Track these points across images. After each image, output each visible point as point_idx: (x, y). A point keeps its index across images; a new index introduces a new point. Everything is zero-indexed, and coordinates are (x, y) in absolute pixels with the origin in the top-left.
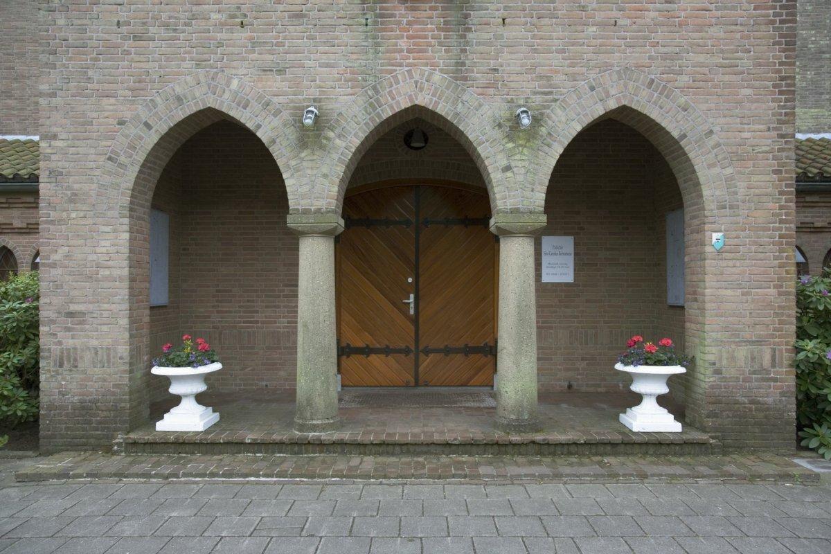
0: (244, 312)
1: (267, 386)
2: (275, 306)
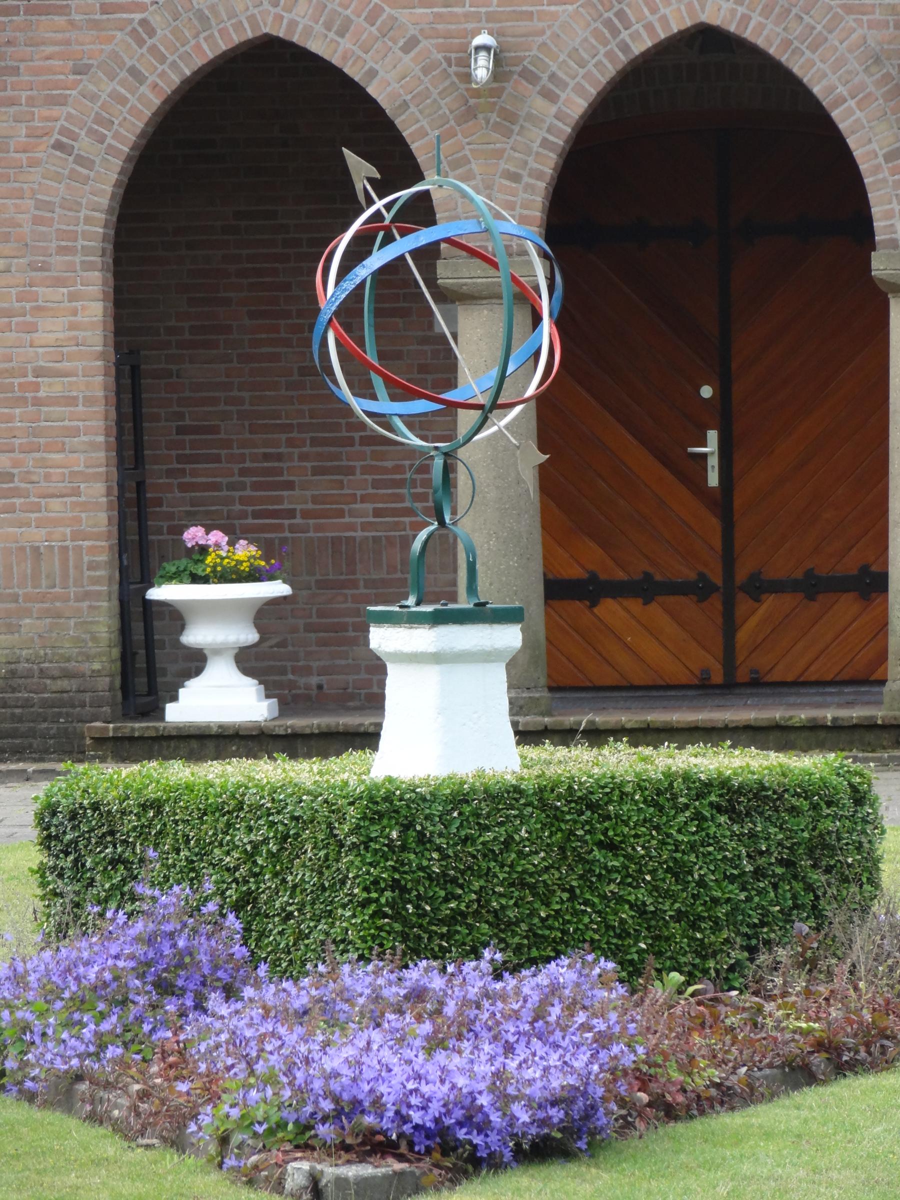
0: (256, 486)
1: (320, 687)
2: (338, 470)
